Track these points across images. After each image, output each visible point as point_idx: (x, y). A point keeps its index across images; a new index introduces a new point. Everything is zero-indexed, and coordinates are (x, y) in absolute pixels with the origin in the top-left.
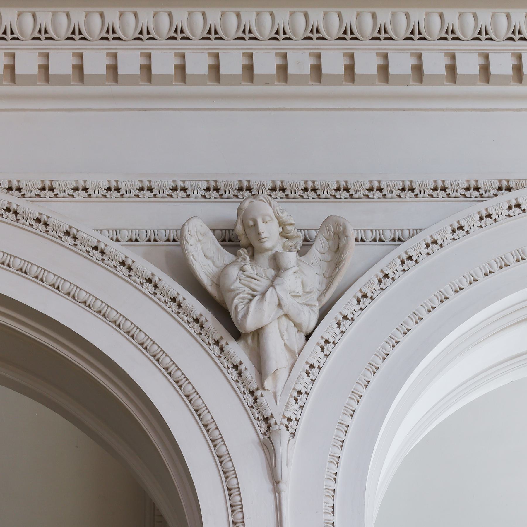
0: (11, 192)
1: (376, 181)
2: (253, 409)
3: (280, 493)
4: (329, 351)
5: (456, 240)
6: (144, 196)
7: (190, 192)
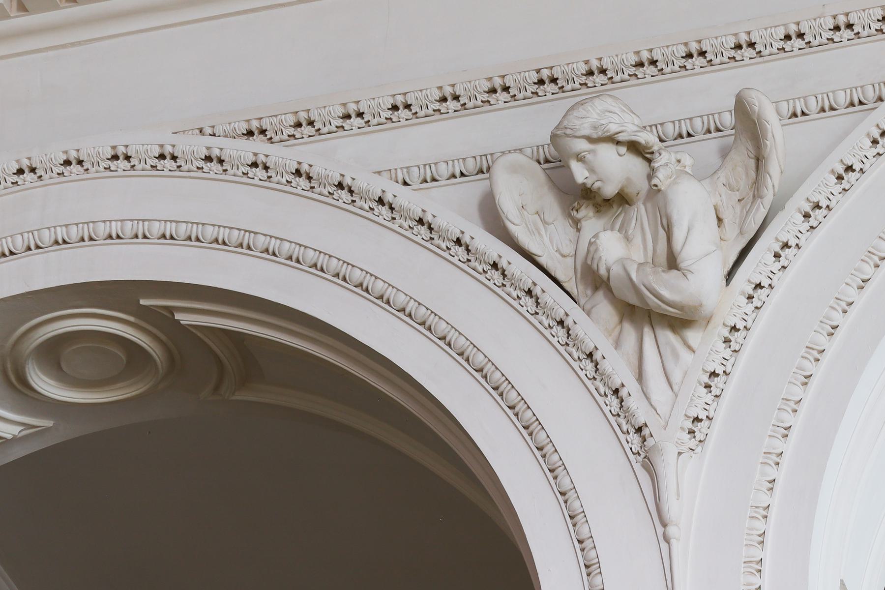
1: (645, 51)
3: (669, 541)
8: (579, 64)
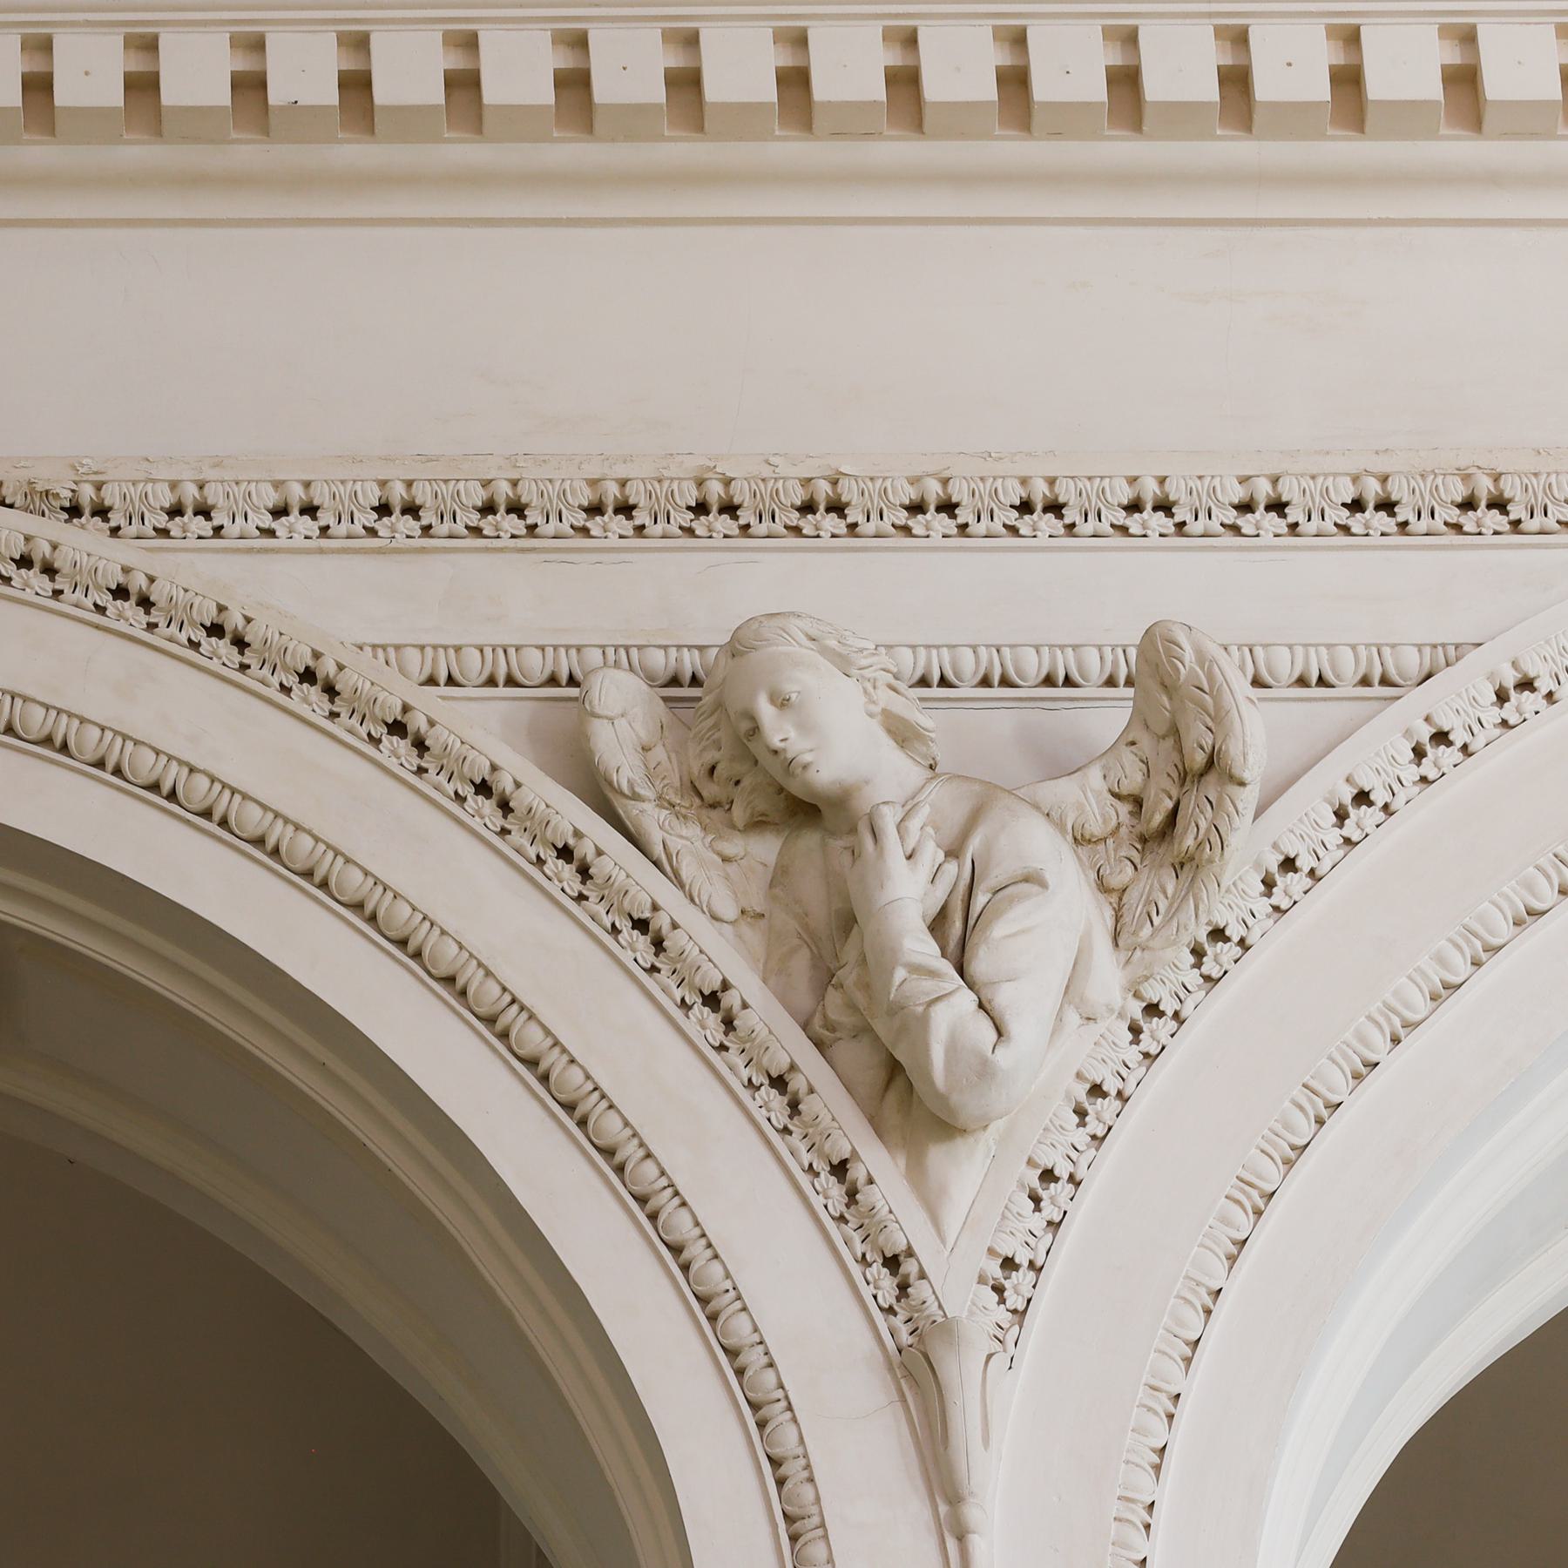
0: (493, 519)
2: (847, 1224)
4: (1159, 1042)
5: (1434, 782)
6: (184, 532)
7: (537, 518)
8: (368, 485)
